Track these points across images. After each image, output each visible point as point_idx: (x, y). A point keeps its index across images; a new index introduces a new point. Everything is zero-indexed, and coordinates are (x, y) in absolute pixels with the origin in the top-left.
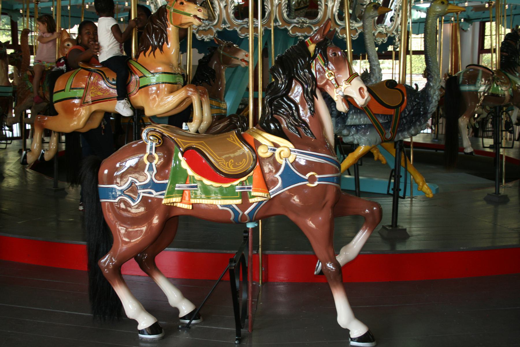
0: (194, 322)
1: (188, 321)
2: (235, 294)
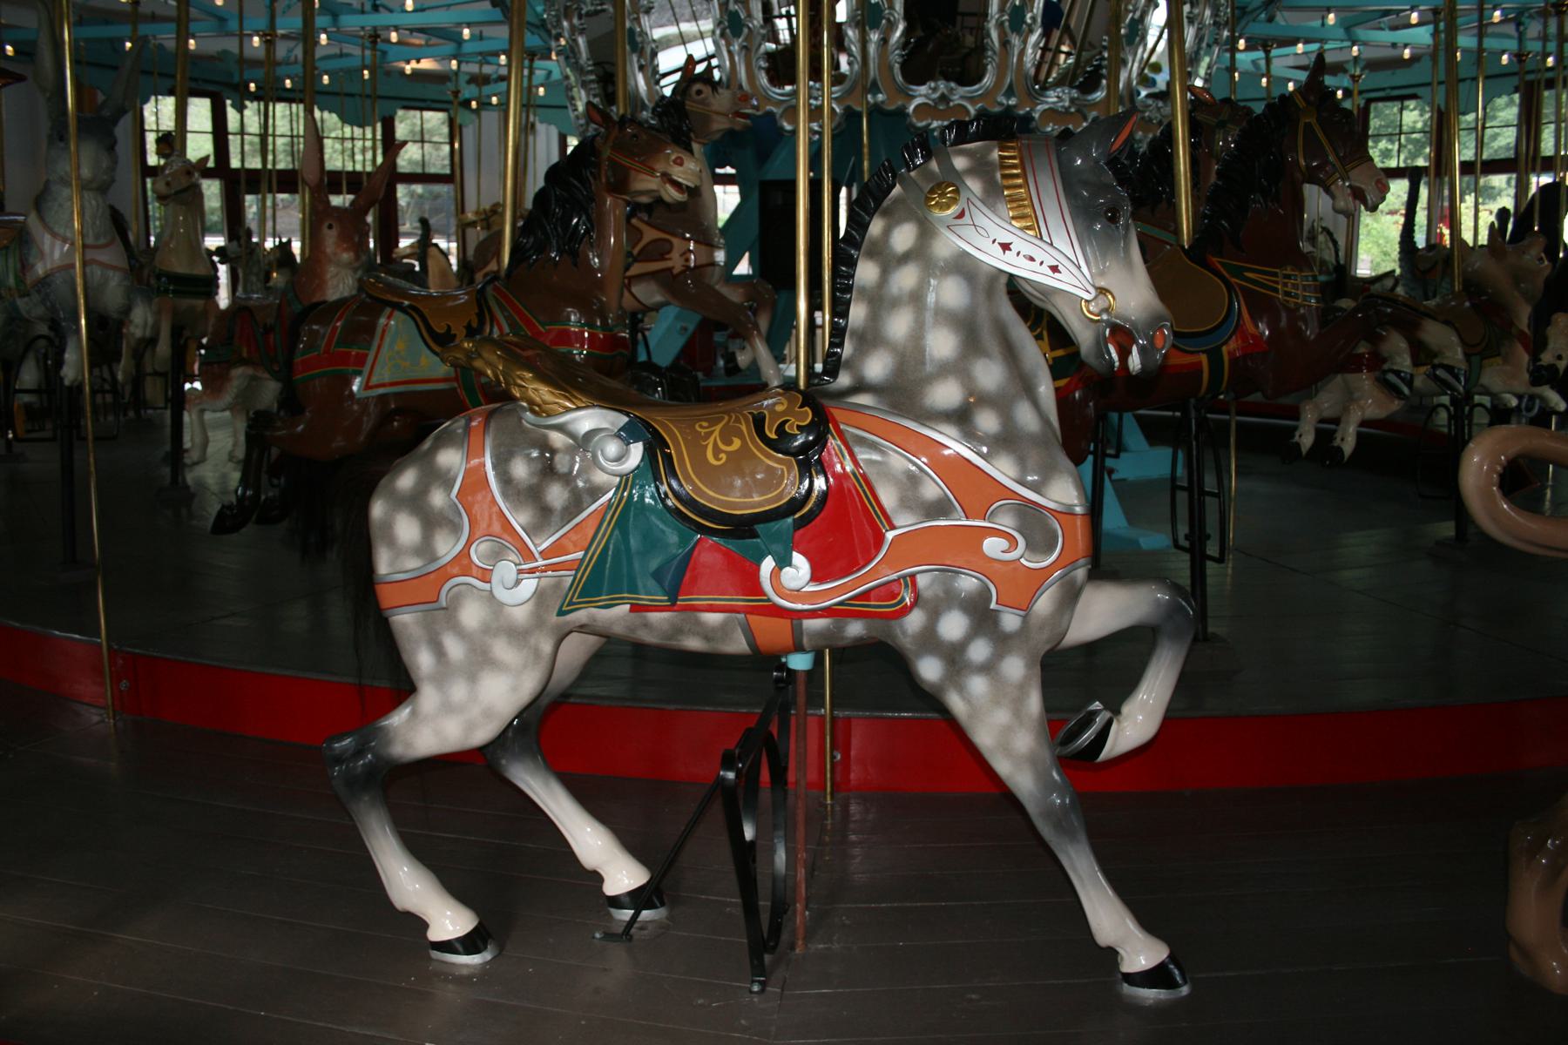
0: (646, 914)
1: (627, 914)
2: (745, 855)
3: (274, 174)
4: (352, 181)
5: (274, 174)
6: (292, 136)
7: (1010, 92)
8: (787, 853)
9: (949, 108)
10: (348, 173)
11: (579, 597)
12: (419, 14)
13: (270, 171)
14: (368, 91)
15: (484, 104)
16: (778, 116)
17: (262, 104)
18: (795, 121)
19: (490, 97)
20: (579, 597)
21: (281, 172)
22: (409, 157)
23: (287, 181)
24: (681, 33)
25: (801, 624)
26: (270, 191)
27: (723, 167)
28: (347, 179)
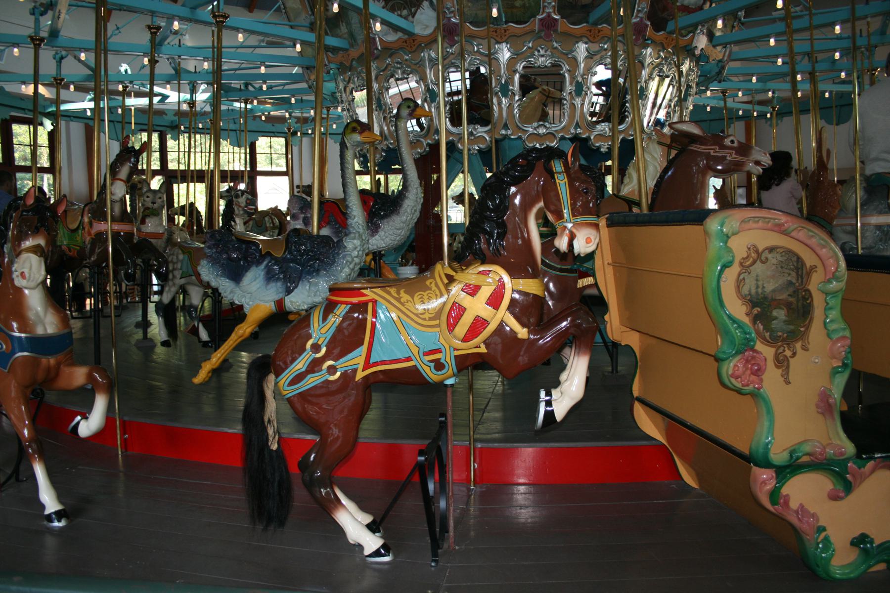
3: (195, 173)
4: (235, 176)
5: (195, 173)
6: (271, 154)
7: (577, 126)
8: (589, 382)
9: (475, 138)
10: (231, 171)
11: (323, 323)
12: (554, 69)
13: (192, 171)
14: (120, 120)
15: (304, 134)
16: (456, 142)
17: (32, 127)
18: (463, 145)
19: (307, 130)
20: (323, 323)
21: (182, 171)
22: (199, 163)
23: (199, 176)
24: (179, 92)
25: (187, 306)
26: (192, 182)
27: (395, 165)
28: (181, 174)
